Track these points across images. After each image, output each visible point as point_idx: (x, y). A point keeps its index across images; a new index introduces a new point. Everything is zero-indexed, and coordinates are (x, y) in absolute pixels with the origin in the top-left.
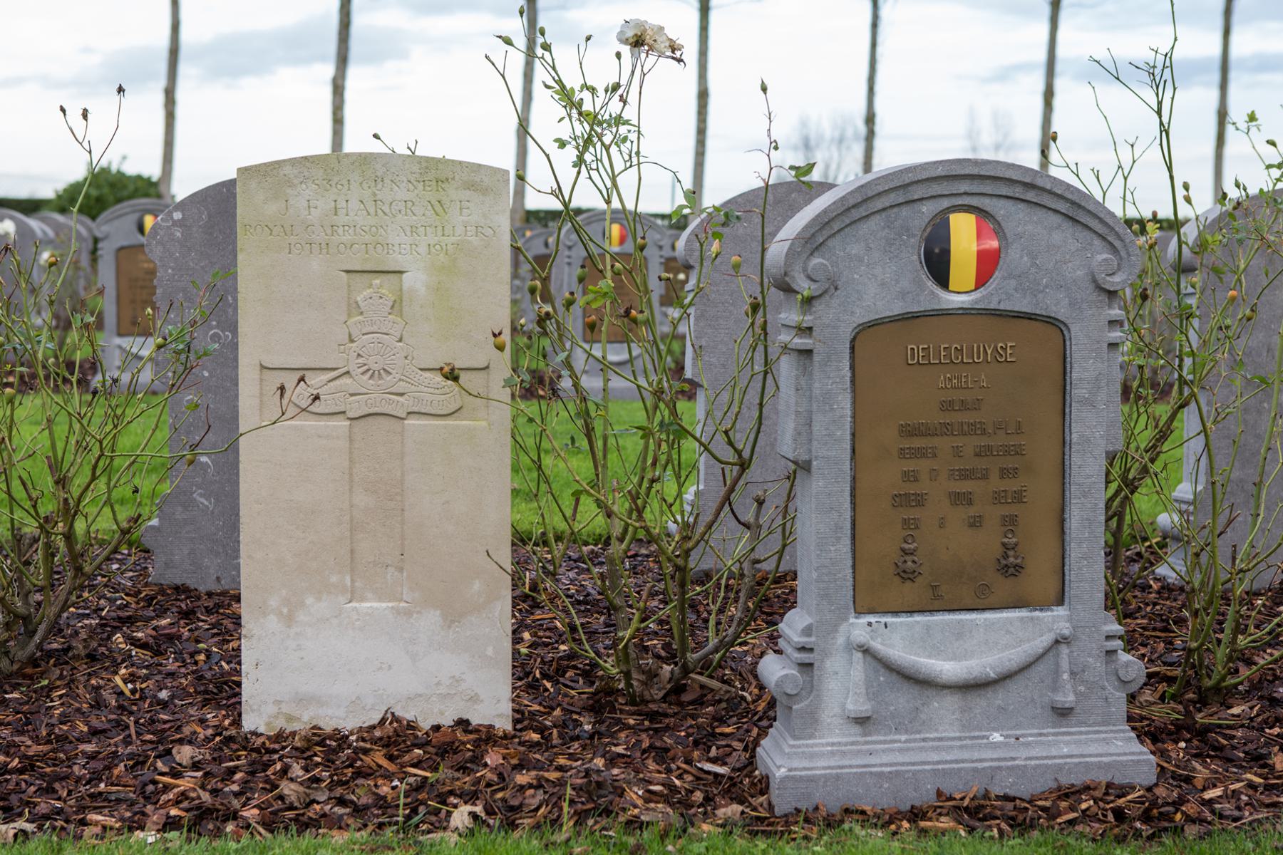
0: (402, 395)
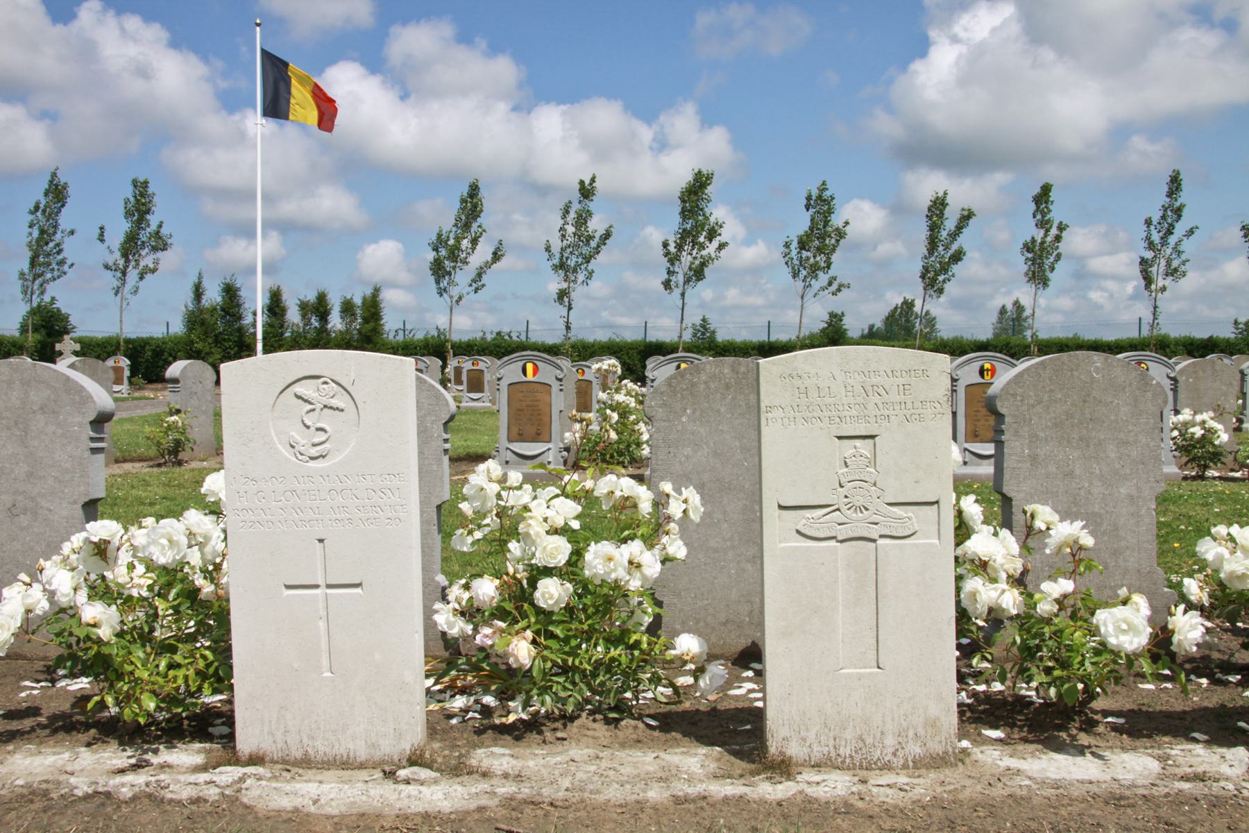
0: (876, 524)
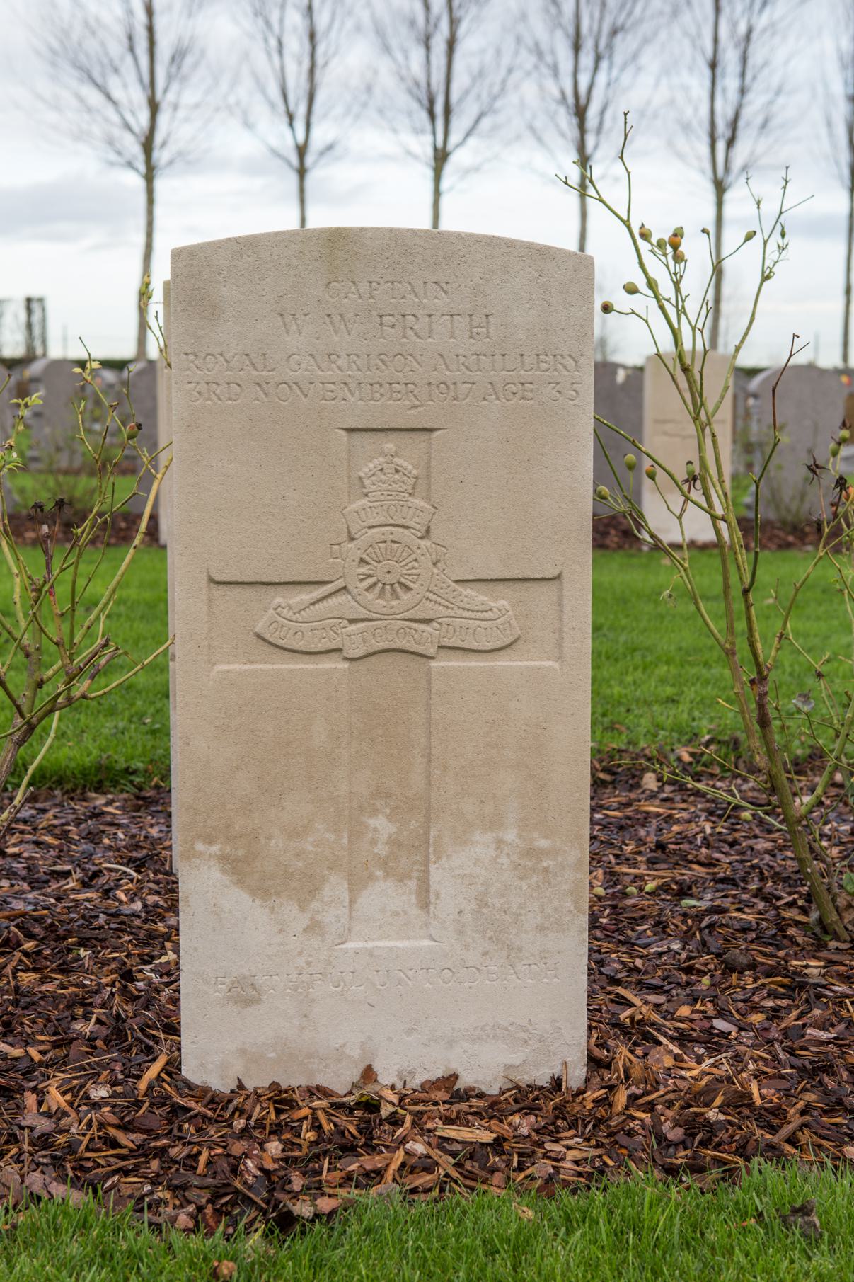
0: (428, 621)
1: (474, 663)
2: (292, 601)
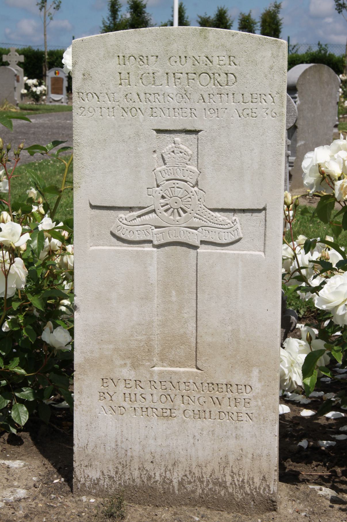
1: (219, 250)
2: (127, 217)
